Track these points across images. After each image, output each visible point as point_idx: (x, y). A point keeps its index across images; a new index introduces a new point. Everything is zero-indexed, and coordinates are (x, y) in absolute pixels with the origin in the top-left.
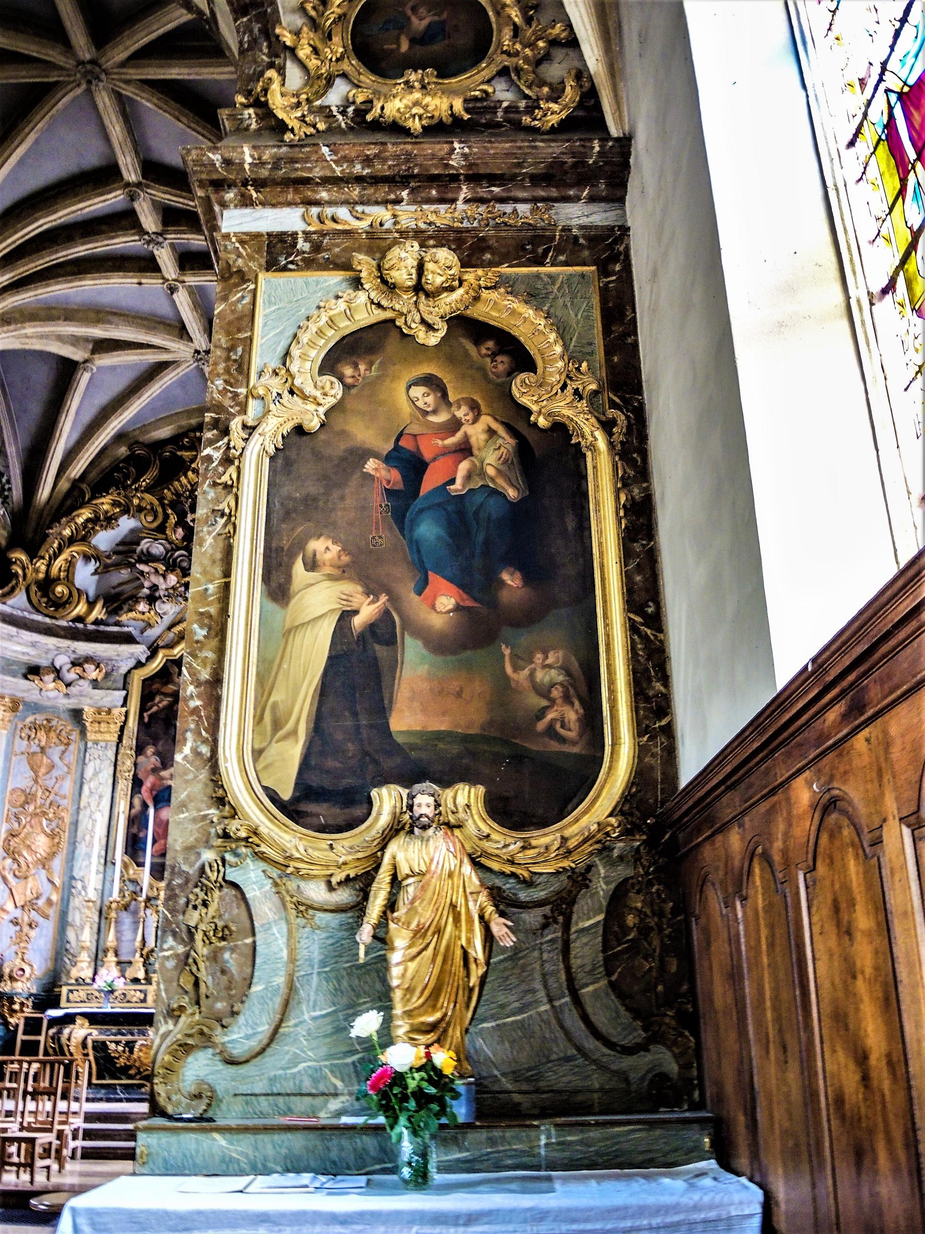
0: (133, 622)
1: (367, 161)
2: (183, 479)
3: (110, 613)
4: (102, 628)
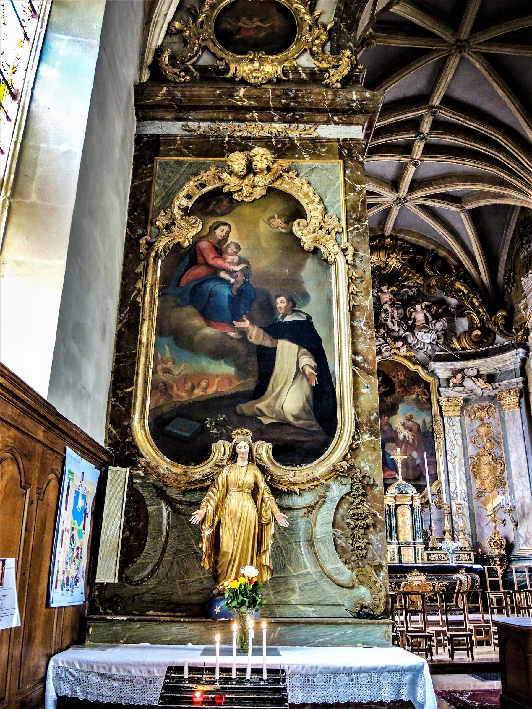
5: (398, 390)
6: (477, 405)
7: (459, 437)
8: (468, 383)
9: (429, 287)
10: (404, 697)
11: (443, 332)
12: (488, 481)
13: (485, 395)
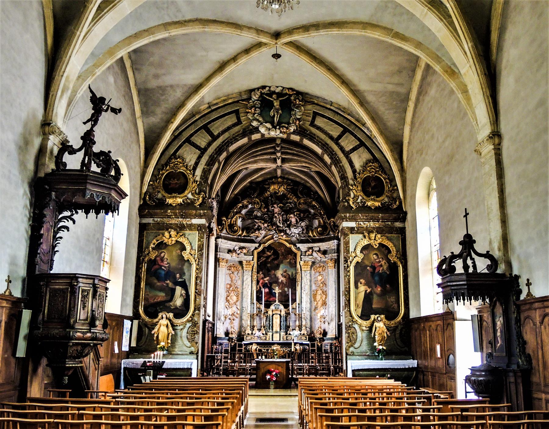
1: (366, 216)
3: (247, 233)
4: (245, 238)
7: (308, 281)
8: (315, 254)
10: (189, 367)
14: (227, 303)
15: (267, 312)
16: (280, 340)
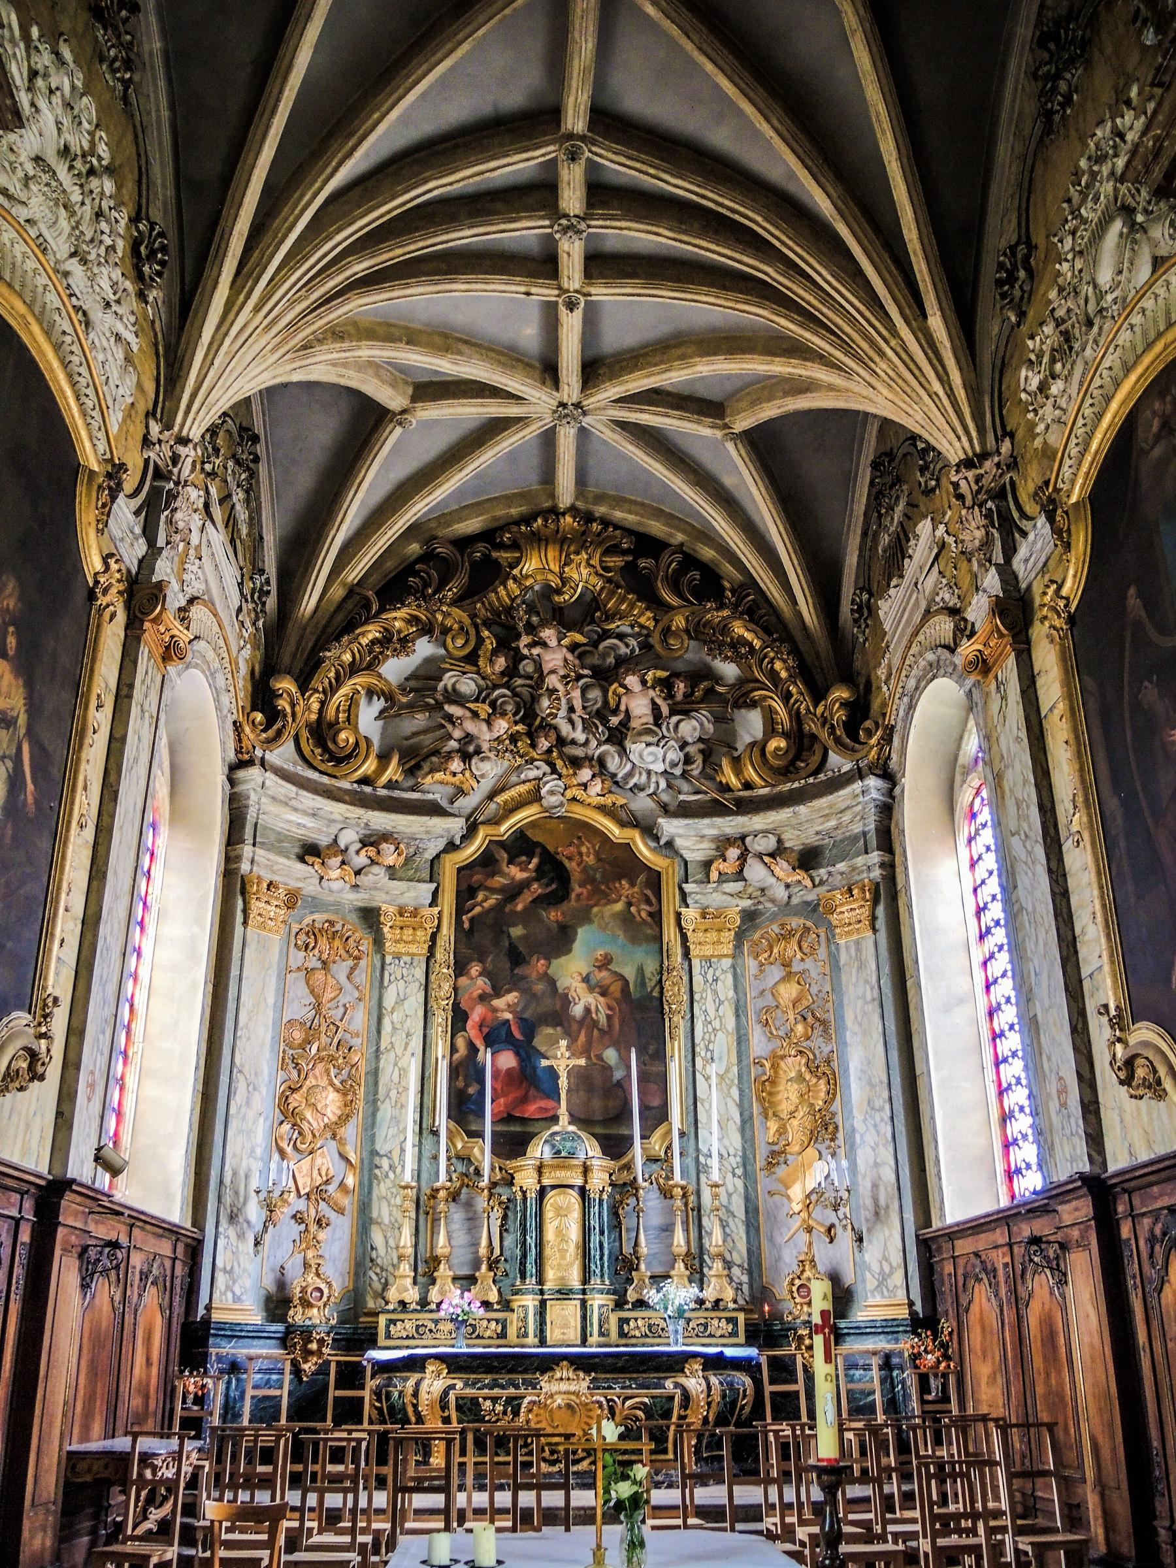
0: (438, 787)
2: (502, 591)
3: (411, 772)
4: (396, 794)
5: (577, 889)
6: (775, 928)
7: (728, 1011)
8: (756, 872)
9: (667, 632)
11: (701, 746)
12: (795, 1122)
13: (795, 901)
14: (286, 1127)
15: (510, 1181)
16: (584, 1342)
